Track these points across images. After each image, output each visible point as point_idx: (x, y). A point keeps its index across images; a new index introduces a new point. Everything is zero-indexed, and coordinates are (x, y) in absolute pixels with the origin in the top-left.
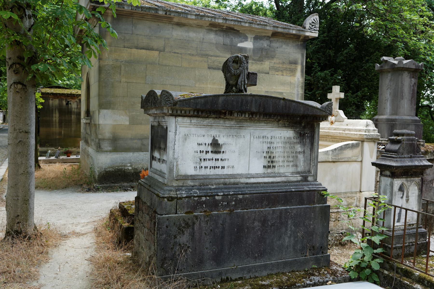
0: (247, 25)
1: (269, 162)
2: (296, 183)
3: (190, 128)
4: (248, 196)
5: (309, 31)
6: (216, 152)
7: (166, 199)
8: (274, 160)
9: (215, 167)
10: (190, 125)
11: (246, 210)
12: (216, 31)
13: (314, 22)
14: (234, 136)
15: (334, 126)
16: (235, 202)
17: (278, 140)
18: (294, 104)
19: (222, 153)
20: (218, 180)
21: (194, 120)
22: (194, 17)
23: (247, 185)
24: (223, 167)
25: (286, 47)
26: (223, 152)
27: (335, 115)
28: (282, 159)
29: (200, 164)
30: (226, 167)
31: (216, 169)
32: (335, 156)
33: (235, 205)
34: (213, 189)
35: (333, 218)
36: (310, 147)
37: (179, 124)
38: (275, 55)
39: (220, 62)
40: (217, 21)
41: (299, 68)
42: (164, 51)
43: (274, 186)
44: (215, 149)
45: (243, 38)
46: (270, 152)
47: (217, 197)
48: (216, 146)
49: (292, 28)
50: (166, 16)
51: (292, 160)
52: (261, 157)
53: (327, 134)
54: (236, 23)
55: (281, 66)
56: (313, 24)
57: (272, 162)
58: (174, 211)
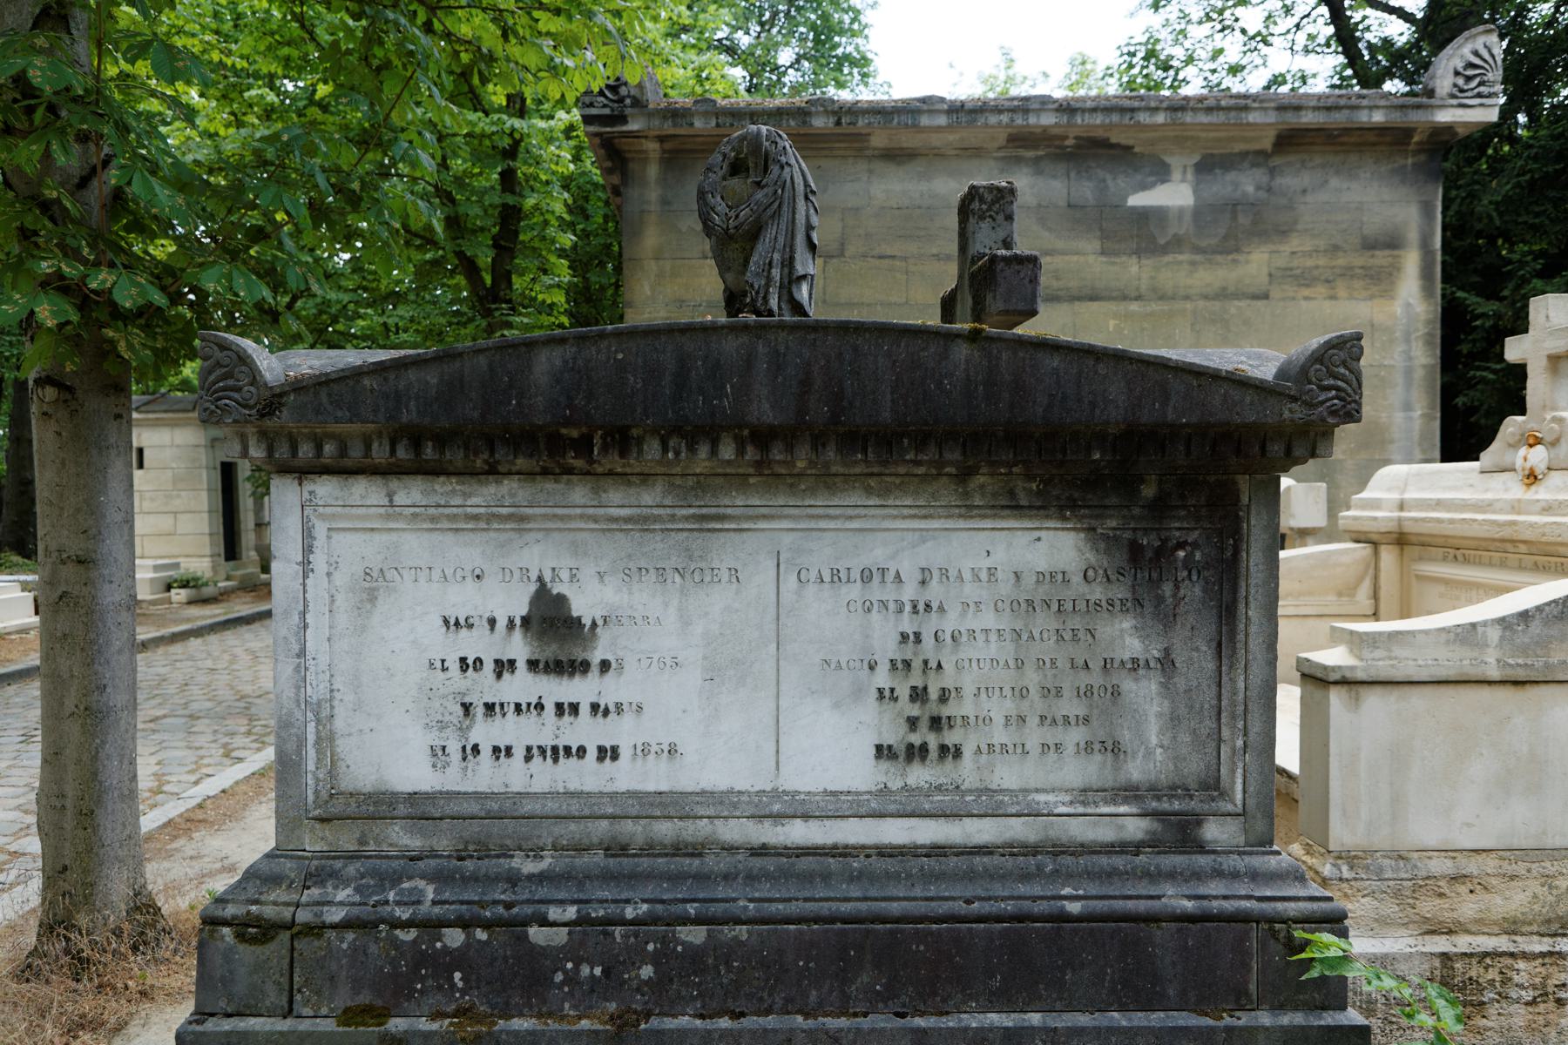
0: (1160, 118)
1: (913, 723)
2: (1104, 861)
3: (394, 537)
4: (742, 931)
5: (1455, 102)
6: (558, 663)
7: (226, 930)
8: (946, 711)
9: (555, 749)
10: (388, 517)
11: (724, 1023)
12: (1038, 159)
13: (1477, 61)
14: (670, 574)
15: (1541, 493)
16: (656, 964)
17: (971, 591)
18: (1055, 361)
19: (595, 669)
20: (573, 826)
21: (411, 493)
22: (942, 120)
23: (757, 862)
24: (608, 753)
25: (1345, 186)
26: (605, 666)
27: (1549, 438)
28: (1009, 706)
29: (463, 731)
30: (625, 753)
31: (568, 765)
32: (1524, 650)
33: (658, 985)
34: (530, 877)
35: (1521, 986)
36: (1209, 629)
37: (322, 517)
38: (1296, 222)
39: (1056, 271)
40: (1032, 120)
41: (1411, 262)
42: (842, 254)
43: (939, 877)
44: (550, 652)
45: (1152, 174)
46: (917, 664)
47: (536, 934)
48: (556, 633)
49: (1365, 102)
50: (838, 130)
51: (1081, 712)
52: (858, 693)
53: (1506, 533)
54: (1115, 118)
55: (1322, 262)
56: (1470, 72)
57: (936, 723)
58: (274, 997)
